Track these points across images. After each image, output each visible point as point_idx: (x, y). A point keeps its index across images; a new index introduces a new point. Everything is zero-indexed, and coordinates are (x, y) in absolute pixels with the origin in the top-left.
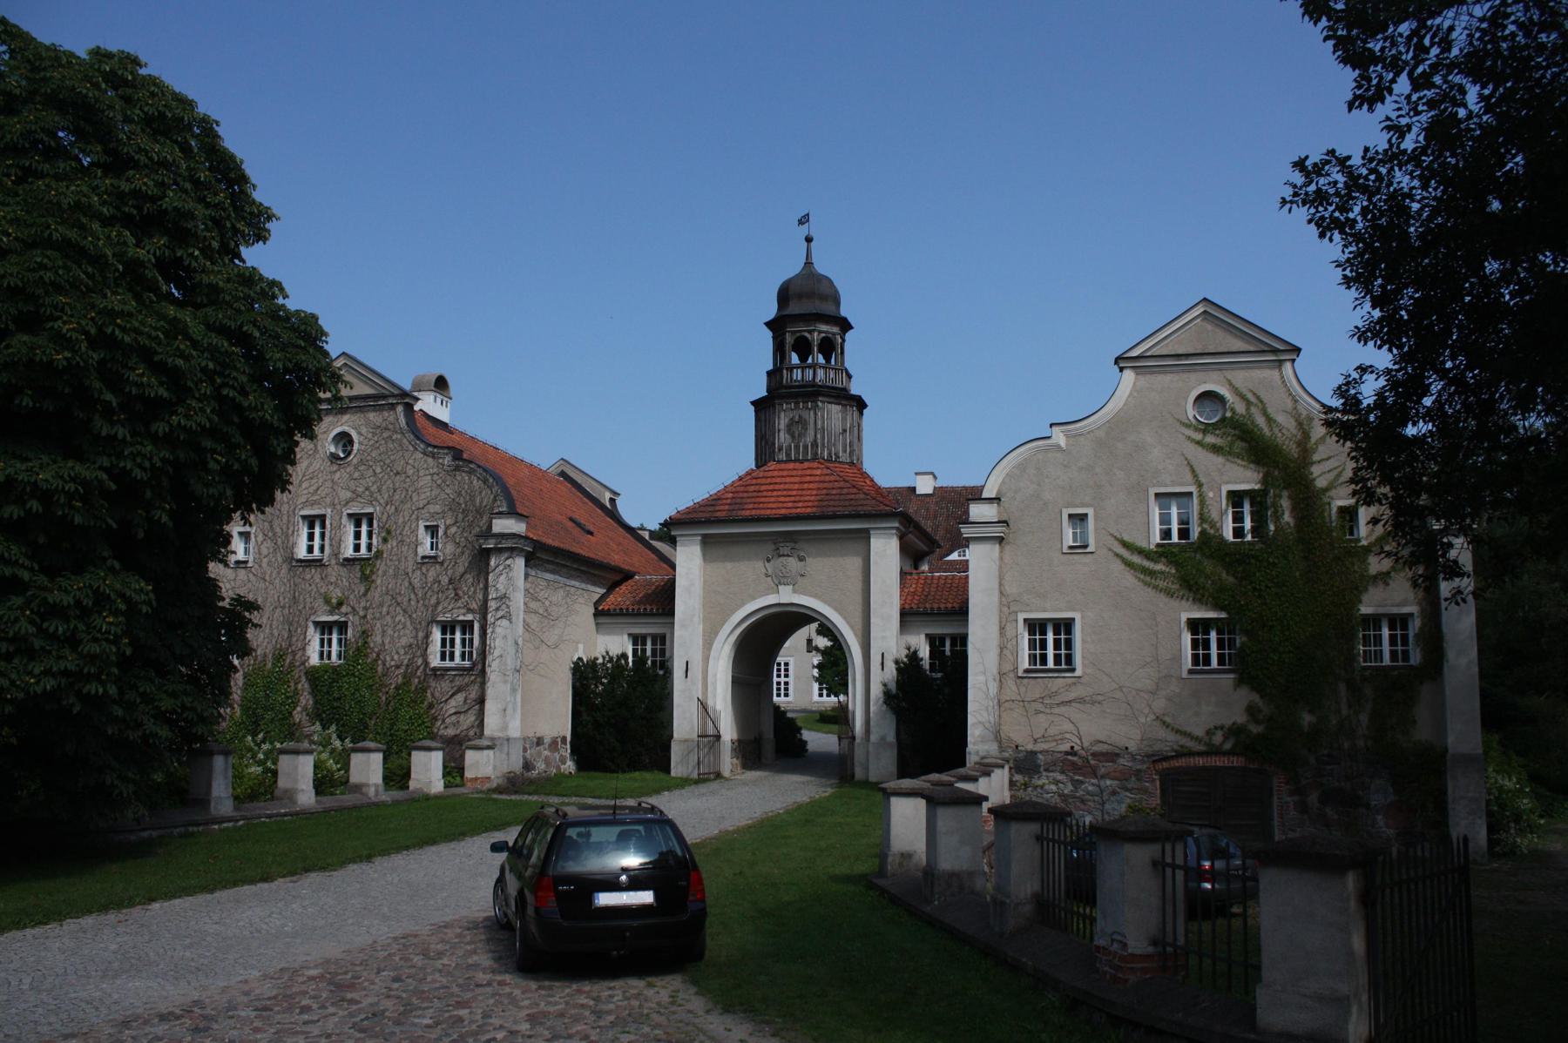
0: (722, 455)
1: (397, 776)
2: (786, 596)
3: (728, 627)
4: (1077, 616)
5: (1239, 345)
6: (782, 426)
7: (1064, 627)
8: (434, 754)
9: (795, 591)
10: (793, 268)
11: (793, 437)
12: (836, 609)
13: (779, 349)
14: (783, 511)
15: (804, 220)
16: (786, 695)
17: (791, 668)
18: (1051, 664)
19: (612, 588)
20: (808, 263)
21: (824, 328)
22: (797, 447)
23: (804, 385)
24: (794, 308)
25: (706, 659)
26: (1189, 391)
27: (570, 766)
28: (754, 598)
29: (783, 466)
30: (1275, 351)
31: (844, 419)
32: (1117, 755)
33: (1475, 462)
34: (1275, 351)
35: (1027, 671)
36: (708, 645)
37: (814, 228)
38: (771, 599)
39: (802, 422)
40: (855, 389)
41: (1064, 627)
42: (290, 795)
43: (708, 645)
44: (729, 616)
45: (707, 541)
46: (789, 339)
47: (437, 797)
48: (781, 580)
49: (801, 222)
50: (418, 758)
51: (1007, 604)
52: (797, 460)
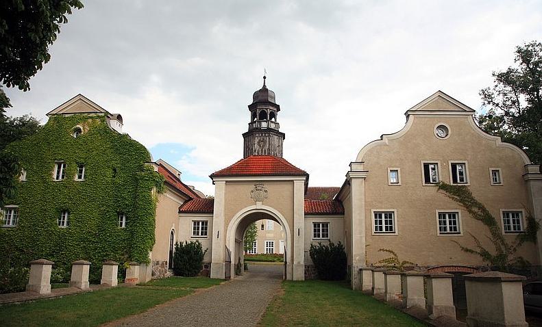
0: (234, 153)
1: (95, 278)
2: (260, 206)
3: (235, 218)
7: (389, 215)
8: (136, 267)
13: (254, 116)
18: (384, 230)
19: (186, 202)
20: (264, 86)
21: (271, 108)
22: (262, 150)
27: (169, 274)
28: (246, 207)
36: (227, 225)
38: (254, 207)
39: (264, 141)
40: (281, 130)
41: (389, 215)
42: (36, 289)
43: (227, 225)
46: (258, 112)
47: (113, 288)
50: (105, 268)
51: (368, 205)
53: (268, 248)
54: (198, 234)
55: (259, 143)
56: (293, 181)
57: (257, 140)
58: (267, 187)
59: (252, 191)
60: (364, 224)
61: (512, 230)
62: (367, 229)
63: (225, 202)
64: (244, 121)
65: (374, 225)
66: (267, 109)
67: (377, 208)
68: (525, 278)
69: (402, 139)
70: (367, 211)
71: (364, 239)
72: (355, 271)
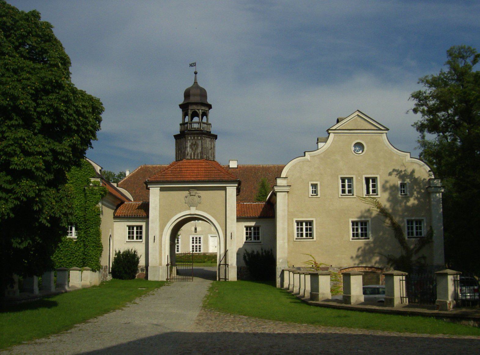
2: (193, 211)
4: (314, 220)
5: (378, 129)
6: (188, 146)
9: (196, 209)
10: (190, 84)
11: (193, 150)
12: (213, 216)
13: (185, 114)
14: (193, 179)
15: (407, 113)
16: (193, 238)
17: (202, 239)
20: (196, 83)
21: (203, 108)
22: (194, 154)
23: (196, 130)
24: (192, 99)
25: (161, 235)
26: (368, 146)
28: (180, 212)
29: (189, 161)
30: (381, 130)
31: (211, 144)
32: (328, 268)
33: (8, 67)
34: (381, 130)
35: (296, 239)
37: (198, 68)
44: (171, 218)
45: (162, 189)
48: (191, 205)
49: (191, 65)
51: (291, 215)
52: (194, 159)
53: (198, 244)
54: (133, 238)
55: (191, 146)
56: (226, 187)
57: (189, 144)
58: (201, 193)
59: (186, 197)
60: (286, 232)
61: (415, 235)
62: (290, 235)
63: (160, 208)
64: (174, 120)
65: (296, 232)
66: (198, 110)
67: (298, 218)
68: (407, 274)
69: (322, 155)
70: (290, 220)
71: (286, 244)
72: (278, 273)
